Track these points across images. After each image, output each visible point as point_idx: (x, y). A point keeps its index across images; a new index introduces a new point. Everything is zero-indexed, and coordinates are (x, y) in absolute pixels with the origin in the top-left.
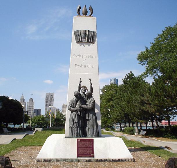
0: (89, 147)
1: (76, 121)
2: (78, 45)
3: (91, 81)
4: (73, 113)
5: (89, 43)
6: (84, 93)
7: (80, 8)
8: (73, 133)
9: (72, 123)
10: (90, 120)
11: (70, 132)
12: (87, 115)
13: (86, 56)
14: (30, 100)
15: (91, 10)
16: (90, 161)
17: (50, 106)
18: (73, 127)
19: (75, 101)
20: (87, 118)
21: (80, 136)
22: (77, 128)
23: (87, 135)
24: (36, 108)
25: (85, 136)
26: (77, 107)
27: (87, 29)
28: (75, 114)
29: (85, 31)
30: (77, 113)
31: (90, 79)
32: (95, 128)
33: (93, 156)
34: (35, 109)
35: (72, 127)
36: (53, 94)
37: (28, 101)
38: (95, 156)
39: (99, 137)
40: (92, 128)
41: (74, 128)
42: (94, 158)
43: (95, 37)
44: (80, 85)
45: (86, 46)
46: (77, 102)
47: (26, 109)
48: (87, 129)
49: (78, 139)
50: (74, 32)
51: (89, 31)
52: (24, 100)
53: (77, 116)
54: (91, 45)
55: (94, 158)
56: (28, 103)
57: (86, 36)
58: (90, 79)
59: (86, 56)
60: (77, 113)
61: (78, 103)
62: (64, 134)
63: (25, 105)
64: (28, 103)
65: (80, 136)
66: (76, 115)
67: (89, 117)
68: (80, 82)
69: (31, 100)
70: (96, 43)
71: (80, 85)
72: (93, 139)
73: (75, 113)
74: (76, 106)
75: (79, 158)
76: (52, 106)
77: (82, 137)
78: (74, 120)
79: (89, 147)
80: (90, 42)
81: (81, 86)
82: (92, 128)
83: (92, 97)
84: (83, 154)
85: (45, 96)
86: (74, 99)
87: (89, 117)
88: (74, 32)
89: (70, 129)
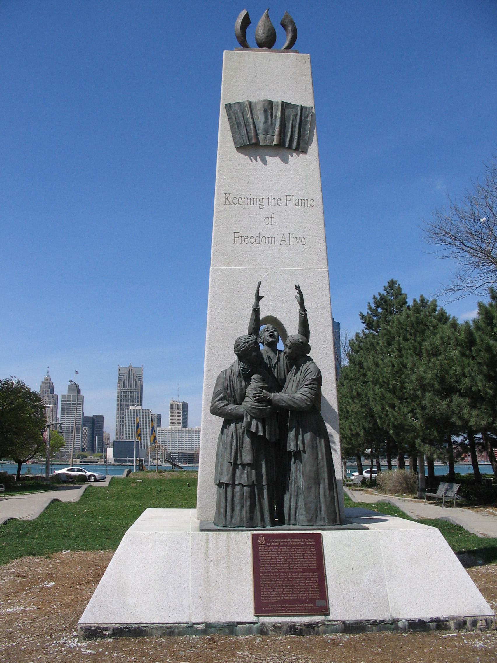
0: (305, 571)
1: (247, 457)
2: (242, 158)
3: (300, 293)
4: (233, 425)
5: (283, 152)
6: (272, 345)
7: (246, 22)
8: (233, 510)
9: (227, 468)
10: (306, 457)
11: (223, 505)
12: (292, 435)
13: (275, 201)
14: (70, 389)
15: (290, 28)
16: (311, 627)
17: (131, 407)
18: (234, 485)
19: (239, 376)
20: (291, 446)
21: (263, 519)
22: (252, 486)
23: (292, 518)
24: (89, 411)
25: (282, 522)
26: (249, 402)
27: (277, 98)
28: (240, 431)
29: (270, 103)
30: (249, 424)
31: (298, 288)
32: (324, 486)
33: (325, 610)
34: (85, 415)
35: (227, 485)
36: (141, 369)
37: (66, 393)
38: (332, 609)
39: (342, 524)
40: (313, 489)
41: (238, 488)
42: (330, 618)
43: (308, 126)
44: (256, 311)
45: (274, 161)
46: (247, 379)
47: (456, 614)
48: (321, 504)
49: (255, 537)
50: (229, 107)
51: (285, 106)
52: (52, 390)
53: (247, 440)
54: (295, 159)
55: (330, 618)
56: (63, 397)
57: (273, 125)
58: (298, 288)
59: (275, 201)
60: (249, 424)
61: (253, 384)
62: (194, 507)
63: (56, 403)
64: (63, 397)
65: (263, 519)
66: (243, 433)
67: (300, 443)
68: (258, 298)
69: (76, 389)
70: (313, 148)
71: (256, 311)
72: (320, 534)
73: (239, 425)
74: (243, 397)
75: (262, 619)
76: (139, 407)
77: (274, 524)
78: (237, 454)
79: (305, 571)
80: (290, 147)
81: (262, 316)
82: (313, 489)
83: (310, 359)
84: (282, 601)
85: (117, 377)
86: (236, 369)
87: (300, 443)
88: (229, 107)
89: (219, 496)
